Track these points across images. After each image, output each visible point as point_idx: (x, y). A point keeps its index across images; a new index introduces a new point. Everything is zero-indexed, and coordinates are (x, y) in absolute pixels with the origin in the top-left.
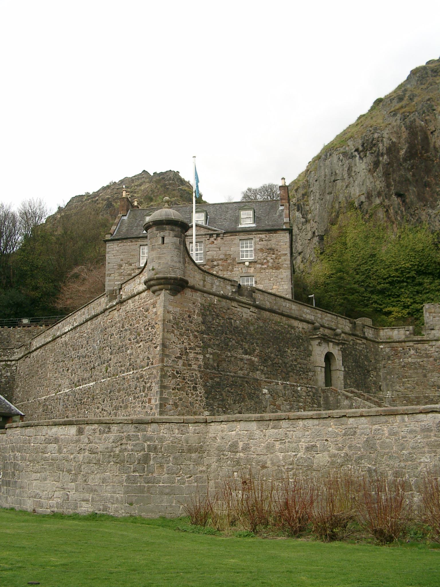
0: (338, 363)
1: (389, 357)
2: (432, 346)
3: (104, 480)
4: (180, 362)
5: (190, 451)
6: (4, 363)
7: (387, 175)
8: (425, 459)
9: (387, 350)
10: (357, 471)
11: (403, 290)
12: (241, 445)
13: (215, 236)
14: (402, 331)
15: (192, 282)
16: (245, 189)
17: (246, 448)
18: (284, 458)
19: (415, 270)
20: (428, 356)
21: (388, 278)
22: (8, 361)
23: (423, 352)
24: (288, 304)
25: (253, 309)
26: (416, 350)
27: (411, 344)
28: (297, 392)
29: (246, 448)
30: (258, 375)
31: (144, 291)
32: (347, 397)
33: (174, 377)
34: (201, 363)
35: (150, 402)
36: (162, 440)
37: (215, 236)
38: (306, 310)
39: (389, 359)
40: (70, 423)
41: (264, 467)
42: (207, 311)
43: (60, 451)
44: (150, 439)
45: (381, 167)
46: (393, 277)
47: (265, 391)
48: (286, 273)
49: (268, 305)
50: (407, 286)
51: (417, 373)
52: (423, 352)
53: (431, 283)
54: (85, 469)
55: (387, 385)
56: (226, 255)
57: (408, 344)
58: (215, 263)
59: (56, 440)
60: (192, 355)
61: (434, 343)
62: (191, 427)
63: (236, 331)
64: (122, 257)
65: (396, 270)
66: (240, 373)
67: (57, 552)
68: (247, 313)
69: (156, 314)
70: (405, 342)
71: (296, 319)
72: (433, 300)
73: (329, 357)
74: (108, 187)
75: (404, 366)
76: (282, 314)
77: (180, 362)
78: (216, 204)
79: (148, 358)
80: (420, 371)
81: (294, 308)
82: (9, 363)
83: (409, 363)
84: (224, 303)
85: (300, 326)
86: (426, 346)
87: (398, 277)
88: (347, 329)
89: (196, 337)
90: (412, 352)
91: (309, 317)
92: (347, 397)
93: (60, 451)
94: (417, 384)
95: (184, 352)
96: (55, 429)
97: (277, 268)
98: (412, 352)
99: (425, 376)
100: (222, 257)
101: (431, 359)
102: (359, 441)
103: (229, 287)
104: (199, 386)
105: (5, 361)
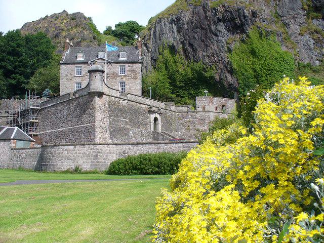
0: (159, 121)
4: (102, 122)
14: (186, 108)
15: (104, 91)
17: (128, 152)
20: (196, 118)
24: (140, 98)
25: (127, 101)
29: (128, 152)
30: (128, 126)
31: (87, 95)
33: (99, 128)
34: (108, 122)
35: (91, 137)
36: (101, 150)
38: (147, 100)
40: (72, 145)
42: (110, 103)
43: (68, 153)
44: (98, 149)
48: (139, 81)
49: (132, 100)
59: (67, 150)
60: (105, 120)
63: (121, 110)
66: (122, 126)
68: (124, 103)
71: (143, 104)
73: (156, 119)
74: (44, 19)
77: (102, 122)
78: (154, 174)
81: (142, 100)
84: (117, 99)
88: (164, 107)
89: (106, 113)
91: (148, 103)
93: (68, 153)
95: (103, 119)
97: (136, 79)
99: (194, 126)
103: (118, 93)
104: (108, 131)
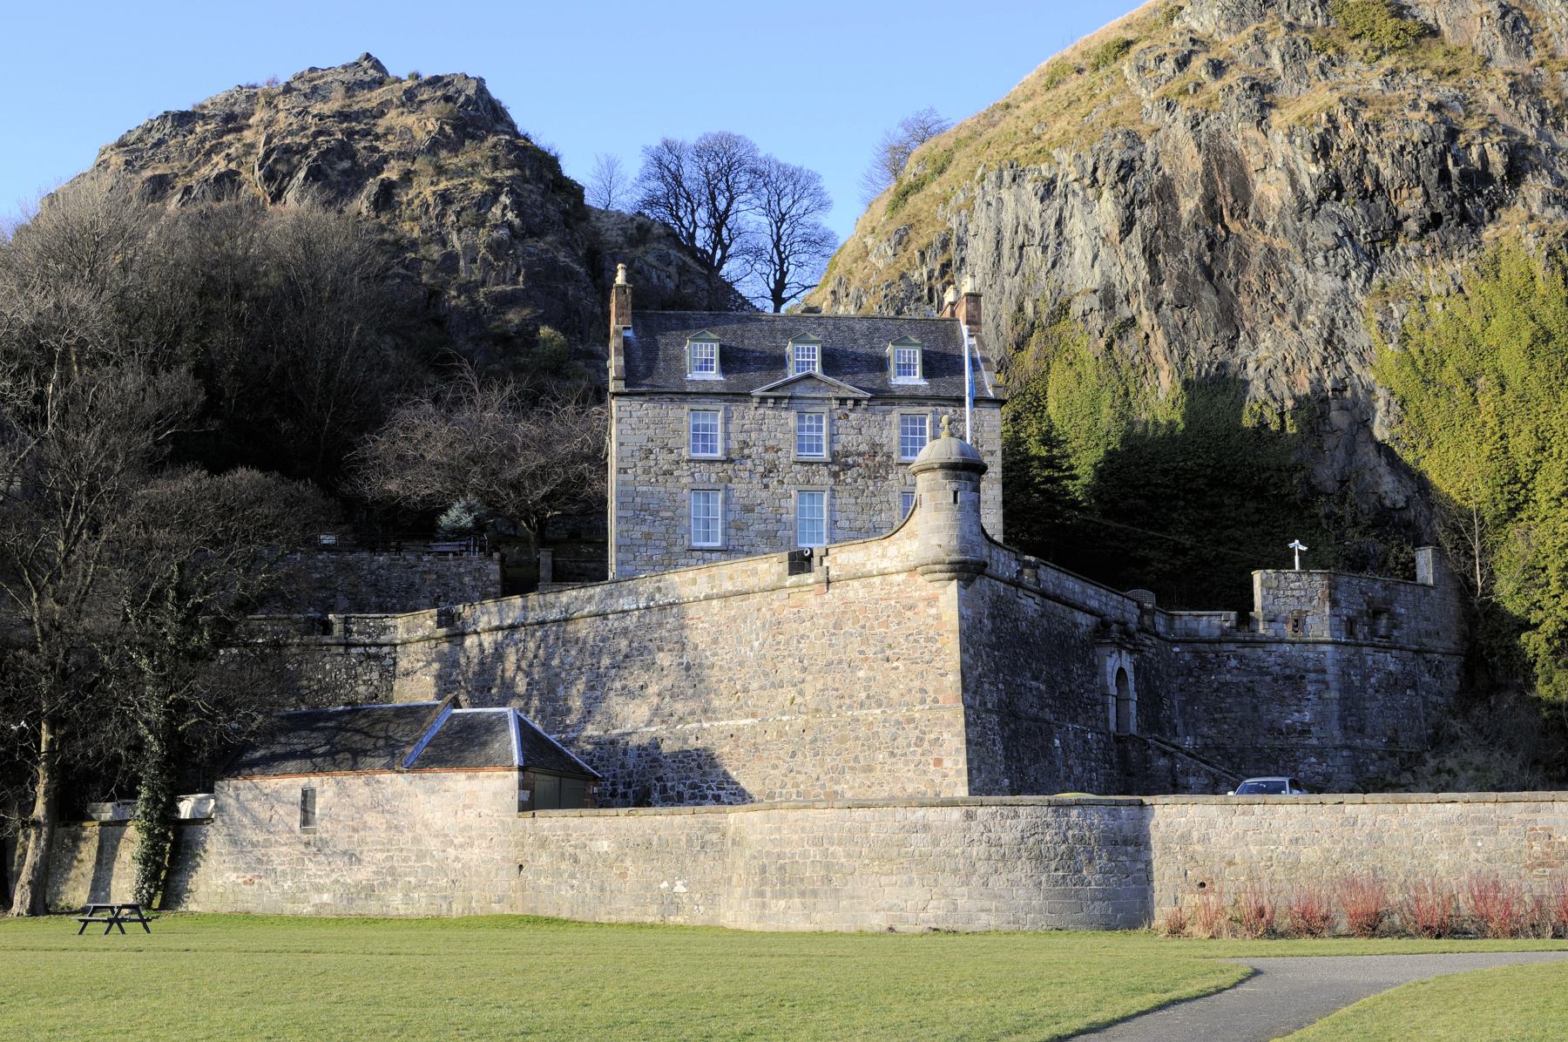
1: (1191, 670)
2: (1270, 653)
3: (1013, 883)
5: (1126, 842)
6: (361, 650)
7: (1151, 255)
8: (1444, 856)
9: (1188, 657)
10: (1359, 869)
11: (1175, 515)
12: (1195, 835)
13: (850, 403)
16: (655, 142)
17: (1204, 839)
18: (1260, 852)
19: (1205, 476)
20: (1263, 671)
21: (1143, 486)
22: (370, 645)
23: (1253, 664)
26: (1240, 658)
27: (1232, 647)
28: (1086, 741)
29: (1204, 839)
32: (1165, 753)
37: (850, 403)
39: (1190, 673)
41: (1231, 863)
45: (1137, 228)
46: (1156, 485)
47: (1057, 742)
50: (1184, 508)
51: (1241, 704)
52: (1253, 664)
53: (1237, 507)
54: (982, 868)
55: (1186, 724)
56: (874, 445)
57: (1225, 647)
58: (850, 460)
59: (926, 828)
61: (1274, 647)
62: (1123, 811)
64: (650, 432)
65: (1165, 472)
67: (523, 1028)
69: (938, 617)
70: (1220, 642)
72: (1241, 544)
75: (1217, 690)
76: (1066, 604)
79: (923, 691)
80: (1247, 700)
82: (373, 650)
83: (1227, 684)
85: (1084, 620)
86: (1260, 651)
87: (1168, 487)
90: (1233, 663)
91: (1094, 604)
92: (1165, 753)
94: (1240, 724)
96: (921, 812)
98: (1233, 663)
99: (1255, 709)
100: (864, 448)
101: (1268, 678)
102: (1360, 835)
105: (365, 645)
